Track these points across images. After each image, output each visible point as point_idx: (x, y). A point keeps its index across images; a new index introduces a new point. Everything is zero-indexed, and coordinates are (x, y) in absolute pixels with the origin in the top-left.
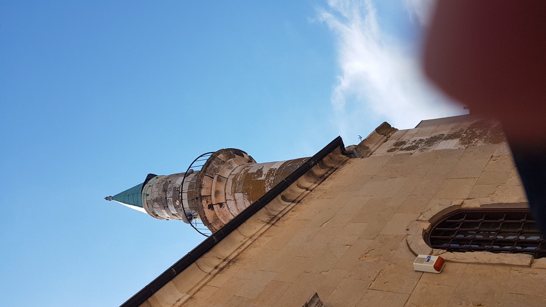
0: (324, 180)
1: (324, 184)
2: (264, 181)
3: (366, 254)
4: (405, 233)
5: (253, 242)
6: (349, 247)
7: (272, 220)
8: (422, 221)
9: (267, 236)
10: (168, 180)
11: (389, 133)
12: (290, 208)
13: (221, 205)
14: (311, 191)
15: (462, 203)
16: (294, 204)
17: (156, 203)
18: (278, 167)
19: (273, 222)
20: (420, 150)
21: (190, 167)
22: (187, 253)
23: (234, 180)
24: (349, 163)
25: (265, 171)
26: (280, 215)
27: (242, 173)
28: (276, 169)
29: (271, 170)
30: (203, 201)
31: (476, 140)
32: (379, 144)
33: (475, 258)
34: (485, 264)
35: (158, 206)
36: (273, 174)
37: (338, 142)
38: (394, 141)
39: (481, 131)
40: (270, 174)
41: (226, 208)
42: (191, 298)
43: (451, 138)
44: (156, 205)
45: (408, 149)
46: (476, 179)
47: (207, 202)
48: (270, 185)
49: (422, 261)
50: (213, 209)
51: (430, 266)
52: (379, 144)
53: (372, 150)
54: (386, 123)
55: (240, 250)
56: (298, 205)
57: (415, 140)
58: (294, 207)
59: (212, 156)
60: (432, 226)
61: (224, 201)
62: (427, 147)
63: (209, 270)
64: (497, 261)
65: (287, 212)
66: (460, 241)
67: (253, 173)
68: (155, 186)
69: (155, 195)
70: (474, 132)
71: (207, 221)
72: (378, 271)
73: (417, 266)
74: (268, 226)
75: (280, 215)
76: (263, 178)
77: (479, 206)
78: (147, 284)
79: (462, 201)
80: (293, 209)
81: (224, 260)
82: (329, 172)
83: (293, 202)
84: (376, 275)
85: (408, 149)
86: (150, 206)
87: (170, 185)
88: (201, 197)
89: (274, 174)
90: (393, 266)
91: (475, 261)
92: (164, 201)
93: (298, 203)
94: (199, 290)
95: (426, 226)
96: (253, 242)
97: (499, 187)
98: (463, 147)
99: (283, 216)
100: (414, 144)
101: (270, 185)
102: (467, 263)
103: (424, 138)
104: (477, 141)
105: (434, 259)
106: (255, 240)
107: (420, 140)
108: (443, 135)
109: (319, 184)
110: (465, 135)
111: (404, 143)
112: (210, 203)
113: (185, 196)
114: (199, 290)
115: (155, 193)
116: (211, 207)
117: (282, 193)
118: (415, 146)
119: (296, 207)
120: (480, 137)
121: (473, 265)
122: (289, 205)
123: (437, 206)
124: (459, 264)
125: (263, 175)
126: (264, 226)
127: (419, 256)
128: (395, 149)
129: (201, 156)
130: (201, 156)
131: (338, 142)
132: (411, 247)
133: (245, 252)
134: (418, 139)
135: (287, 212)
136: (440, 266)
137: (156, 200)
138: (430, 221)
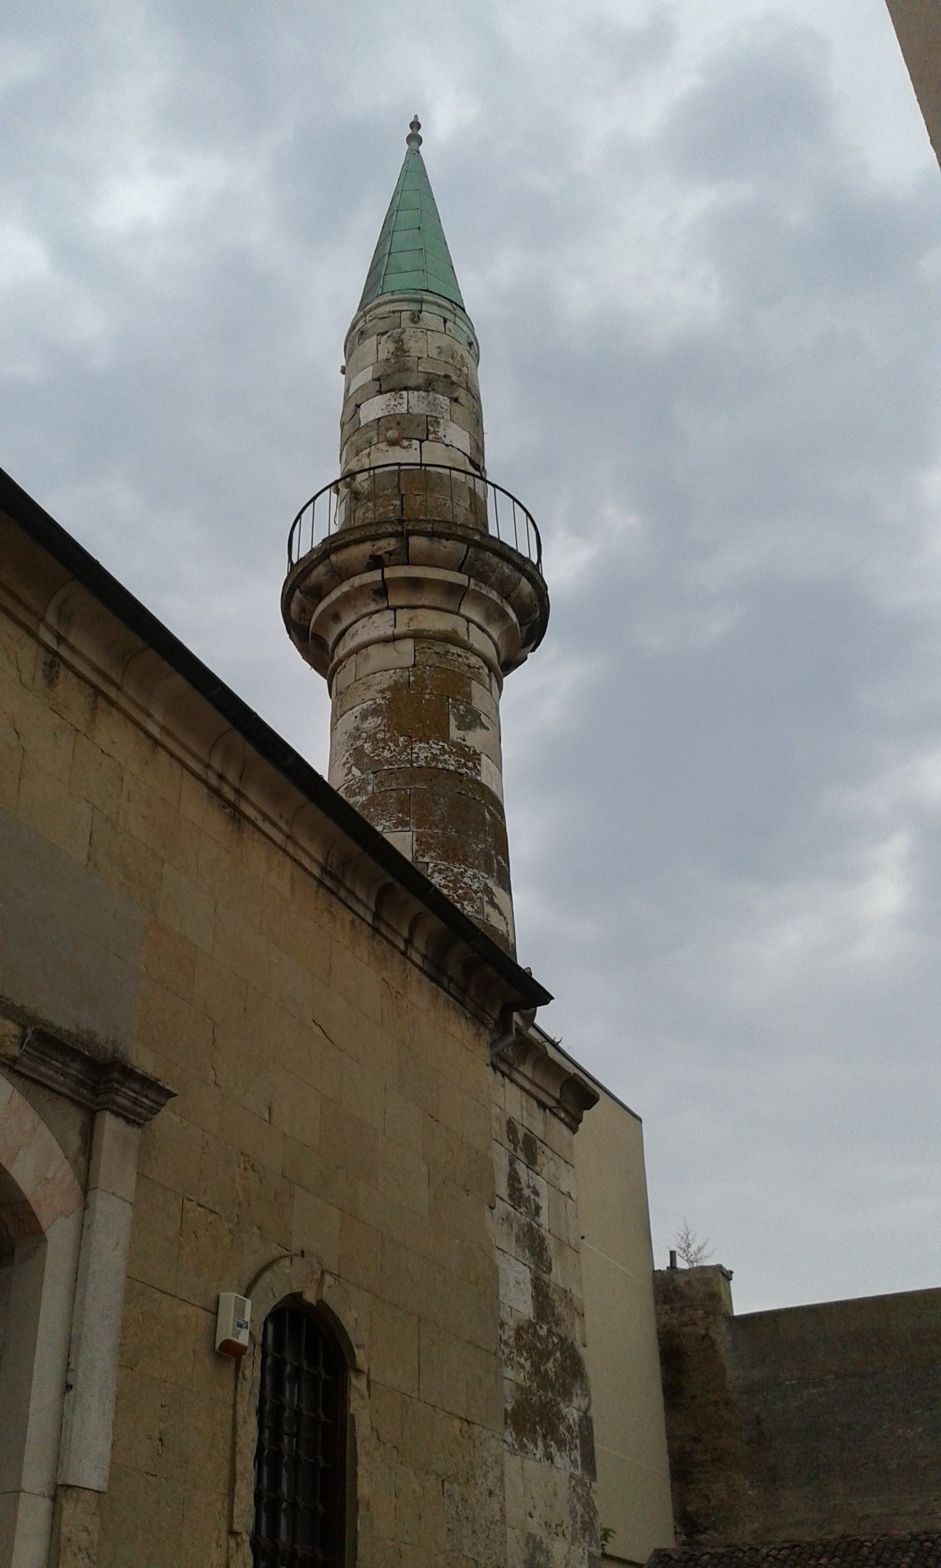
0: (432, 978)
1: (420, 982)
2: (445, 737)
3: (252, 1166)
4: (295, 1248)
5: (280, 847)
6: (267, 1117)
7: (333, 877)
8: (321, 1283)
9: (292, 878)
10: (461, 394)
11: (566, 1111)
12: (361, 910)
13: (382, 591)
14: (404, 954)
15: (359, 1371)
16: (369, 919)
17: (391, 347)
18: (484, 778)
19: (328, 882)
20: (509, 1214)
21: (495, 486)
22: (254, 710)
23: (449, 638)
24: (478, 1035)
25: (474, 739)
26: (343, 893)
27: (474, 660)
28: (479, 773)
29: (475, 757)
30: (393, 541)
31: (528, 1365)
32: (534, 1090)
33: (245, 1422)
34: (234, 1444)
35: (383, 355)
36: (465, 765)
37: (544, 997)
38: (539, 1130)
39: (552, 1375)
40: (462, 756)
41: (373, 607)
42: (156, 742)
43: (538, 1295)
44: (387, 347)
45: (513, 1178)
46: (415, 1395)
47: (390, 553)
48: (435, 757)
49: (240, 1310)
50: (370, 568)
51: (226, 1331)
52: (534, 1090)
53: (516, 1076)
54: (598, 1100)
55: (260, 823)
56: (367, 931)
57: (536, 1193)
58: (363, 920)
59: (528, 560)
60: (310, 1306)
61: (393, 602)
62: (515, 1230)
63: (216, 764)
64: (240, 1466)
65: (350, 908)
66: (279, 1364)
67: (469, 696)
68: (444, 341)
69: (415, 345)
70: (550, 1354)
71: (337, 549)
72: (217, 1209)
73: (229, 1299)
74: (316, 871)
75: (343, 893)
76: (455, 734)
77: (352, 1410)
78: (185, 644)
79: (365, 1368)
80: (358, 921)
81: (237, 791)
82: (452, 986)
83: (376, 916)
84: (210, 1205)
85: (513, 1178)
86: (382, 326)
87: (444, 401)
88: (403, 537)
89: (464, 770)
90: (227, 1241)
91: (240, 1420)
92: (397, 378)
93: (373, 928)
94: (172, 755)
95: (310, 1297)
96: (280, 847)
97: (395, 1451)
98: (508, 1334)
99: (340, 899)
100: (527, 1192)
101: (435, 757)
102: (234, 1405)
103: (544, 1218)
104: (522, 1366)
105: (243, 1339)
106: (284, 850)
107: (538, 1208)
108: (549, 1270)
109: (420, 969)
110: (543, 1332)
111: (532, 1161)
112: (387, 562)
113: (409, 455)
114: (172, 755)
115: (422, 344)
116: (376, 562)
117: (398, 885)
118: (521, 1196)
119: (364, 925)
120: (537, 1372)
121: (230, 1418)
122: (366, 906)
123: (353, 1316)
124: (232, 1386)
125: (461, 733)
126: (315, 860)
127: (249, 1303)
128: (514, 1141)
129: (528, 515)
130: (528, 515)
131: (544, 997)
132: (268, 1276)
133: (257, 835)
134: (544, 1203)
135: (350, 908)
136: (230, 1352)
137: (401, 350)
138: (321, 1302)
